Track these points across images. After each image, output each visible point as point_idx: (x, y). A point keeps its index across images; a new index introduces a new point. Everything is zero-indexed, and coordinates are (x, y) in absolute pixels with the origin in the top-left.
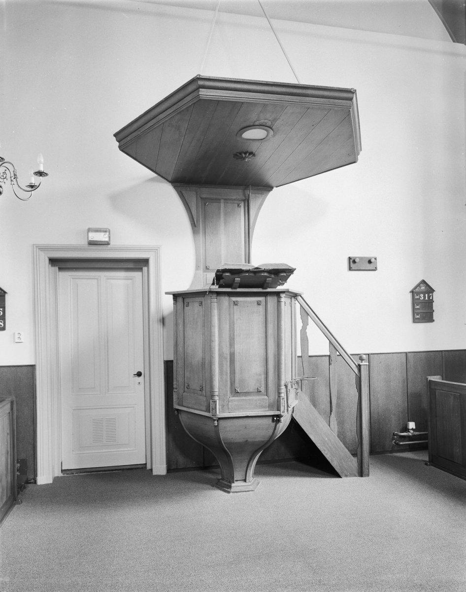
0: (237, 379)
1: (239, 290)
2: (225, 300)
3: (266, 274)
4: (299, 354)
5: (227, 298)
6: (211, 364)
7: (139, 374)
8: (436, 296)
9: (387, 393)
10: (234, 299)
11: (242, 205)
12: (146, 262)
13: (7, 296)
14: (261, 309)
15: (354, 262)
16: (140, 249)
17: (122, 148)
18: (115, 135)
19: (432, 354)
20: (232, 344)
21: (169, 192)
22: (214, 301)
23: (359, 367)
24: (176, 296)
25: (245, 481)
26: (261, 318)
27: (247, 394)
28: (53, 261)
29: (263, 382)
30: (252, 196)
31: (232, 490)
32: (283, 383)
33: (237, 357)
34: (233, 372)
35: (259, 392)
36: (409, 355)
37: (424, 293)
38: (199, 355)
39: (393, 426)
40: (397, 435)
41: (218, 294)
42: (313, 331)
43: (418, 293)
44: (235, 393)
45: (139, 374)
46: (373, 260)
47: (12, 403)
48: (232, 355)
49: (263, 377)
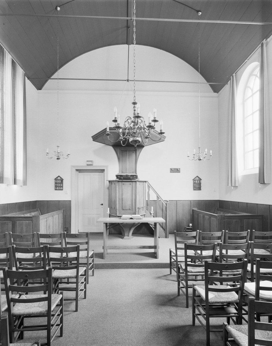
0: (124, 206)
1: (124, 180)
2: (120, 183)
3: (130, 176)
4: (147, 199)
5: (121, 182)
6: (116, 201)
7: (102, 204)
8: (202, 182)
9: (184, 214)
10: (123, 183)
11: (134, 152)
12: (104, 170)
13: (63, 180)
14: (131, 186)
15: (172, 170)
16: (100, 166)
17: (94, 140)
18: (92, 137)
19: (200, 201)
20: (122, 194)
21: (111, 149)
22: (117, 184)
23: (166, 204)
24: (109, 181)
25: (128, 236)
26: (131, 189)
27: (126, 210)
28: (77, 170)
29: (131, 207)
30: (137, 149)
31: (124, 238)
32: (137, 207)
33: (124, 199)
34: (122, 204)
35: (130, 209)
36: (191, 201)
37: (197, 180)
38: (114, 200)
39: (185, 224)
40: (186, 228)
41: (118, 181)
42: (151, 192)
43: (195, 180)
44: (123, 210)
45: (102, 204)
46: (178, 169)
47: (64, 210)
48: (122, 199)
49: (131, 205)
